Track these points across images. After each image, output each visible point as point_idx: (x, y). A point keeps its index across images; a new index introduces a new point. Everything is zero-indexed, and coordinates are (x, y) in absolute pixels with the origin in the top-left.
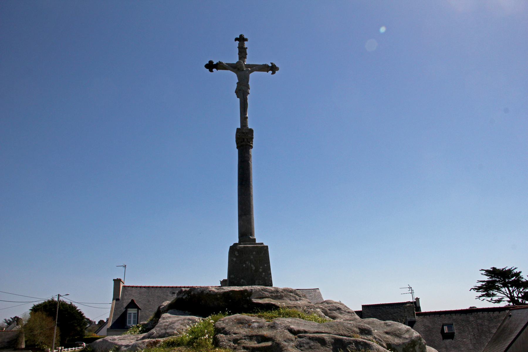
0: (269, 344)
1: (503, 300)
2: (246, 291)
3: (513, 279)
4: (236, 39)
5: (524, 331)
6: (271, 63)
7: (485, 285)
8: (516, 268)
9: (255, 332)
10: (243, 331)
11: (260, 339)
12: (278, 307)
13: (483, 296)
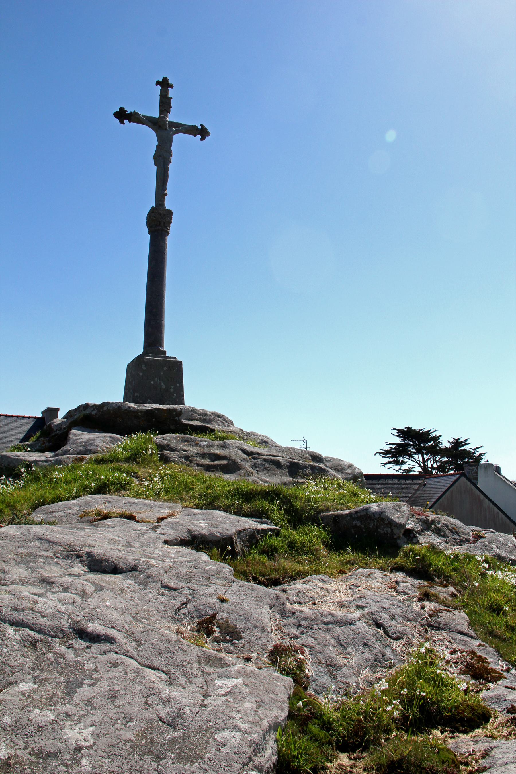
0: (225, 462)
1: (414, 469)
2: (175, 410)
3: (430, 444)
4: (158, 83)
5: (439, 502)
6: (202, 125)
7: (395, 448)
8: (436, 431)
9: (206, 450)
10: (192, 449)
11: (213, 457)
12: (214, 430)
13: (390, 463)
